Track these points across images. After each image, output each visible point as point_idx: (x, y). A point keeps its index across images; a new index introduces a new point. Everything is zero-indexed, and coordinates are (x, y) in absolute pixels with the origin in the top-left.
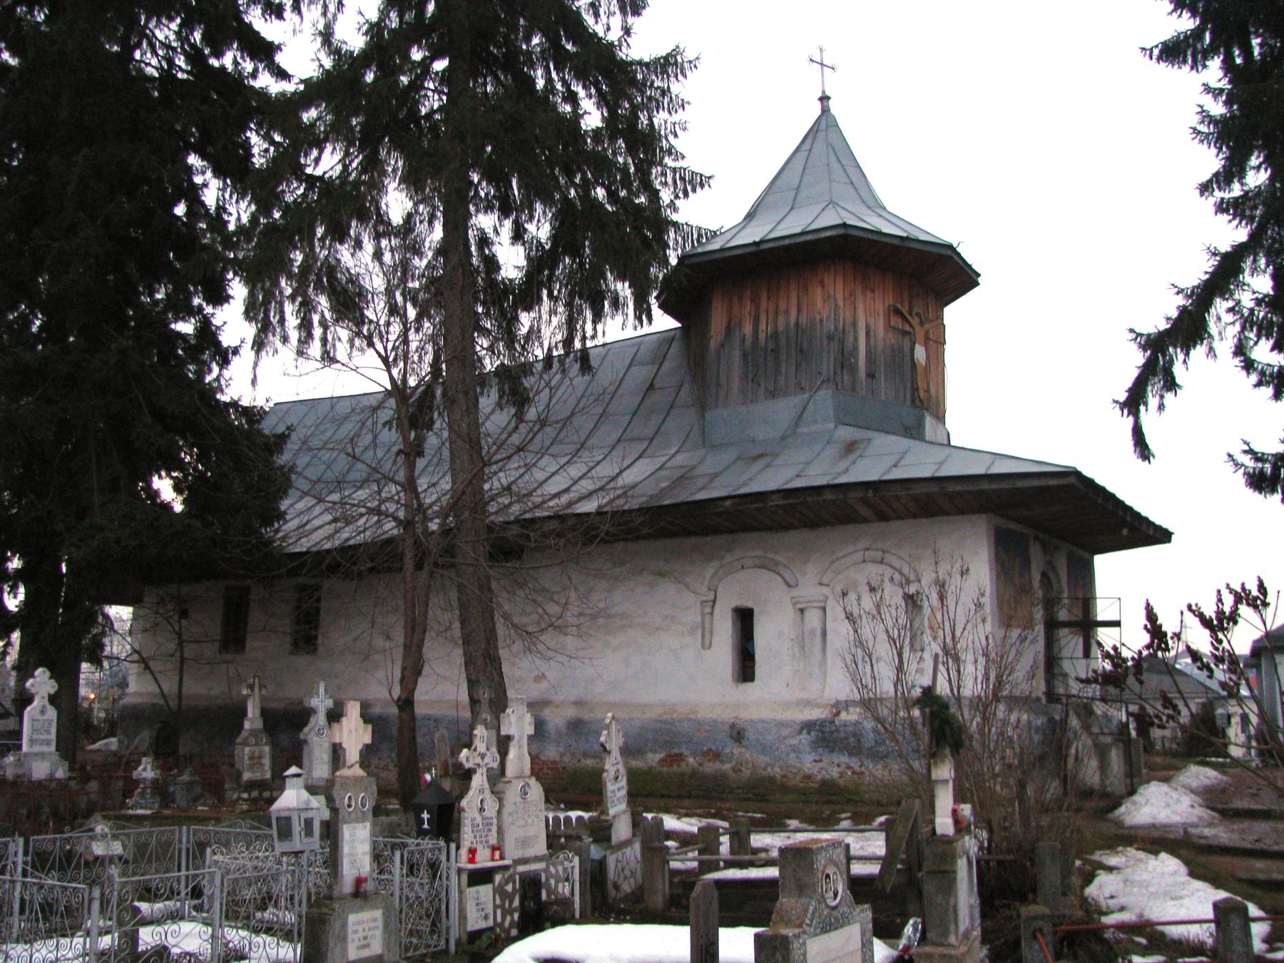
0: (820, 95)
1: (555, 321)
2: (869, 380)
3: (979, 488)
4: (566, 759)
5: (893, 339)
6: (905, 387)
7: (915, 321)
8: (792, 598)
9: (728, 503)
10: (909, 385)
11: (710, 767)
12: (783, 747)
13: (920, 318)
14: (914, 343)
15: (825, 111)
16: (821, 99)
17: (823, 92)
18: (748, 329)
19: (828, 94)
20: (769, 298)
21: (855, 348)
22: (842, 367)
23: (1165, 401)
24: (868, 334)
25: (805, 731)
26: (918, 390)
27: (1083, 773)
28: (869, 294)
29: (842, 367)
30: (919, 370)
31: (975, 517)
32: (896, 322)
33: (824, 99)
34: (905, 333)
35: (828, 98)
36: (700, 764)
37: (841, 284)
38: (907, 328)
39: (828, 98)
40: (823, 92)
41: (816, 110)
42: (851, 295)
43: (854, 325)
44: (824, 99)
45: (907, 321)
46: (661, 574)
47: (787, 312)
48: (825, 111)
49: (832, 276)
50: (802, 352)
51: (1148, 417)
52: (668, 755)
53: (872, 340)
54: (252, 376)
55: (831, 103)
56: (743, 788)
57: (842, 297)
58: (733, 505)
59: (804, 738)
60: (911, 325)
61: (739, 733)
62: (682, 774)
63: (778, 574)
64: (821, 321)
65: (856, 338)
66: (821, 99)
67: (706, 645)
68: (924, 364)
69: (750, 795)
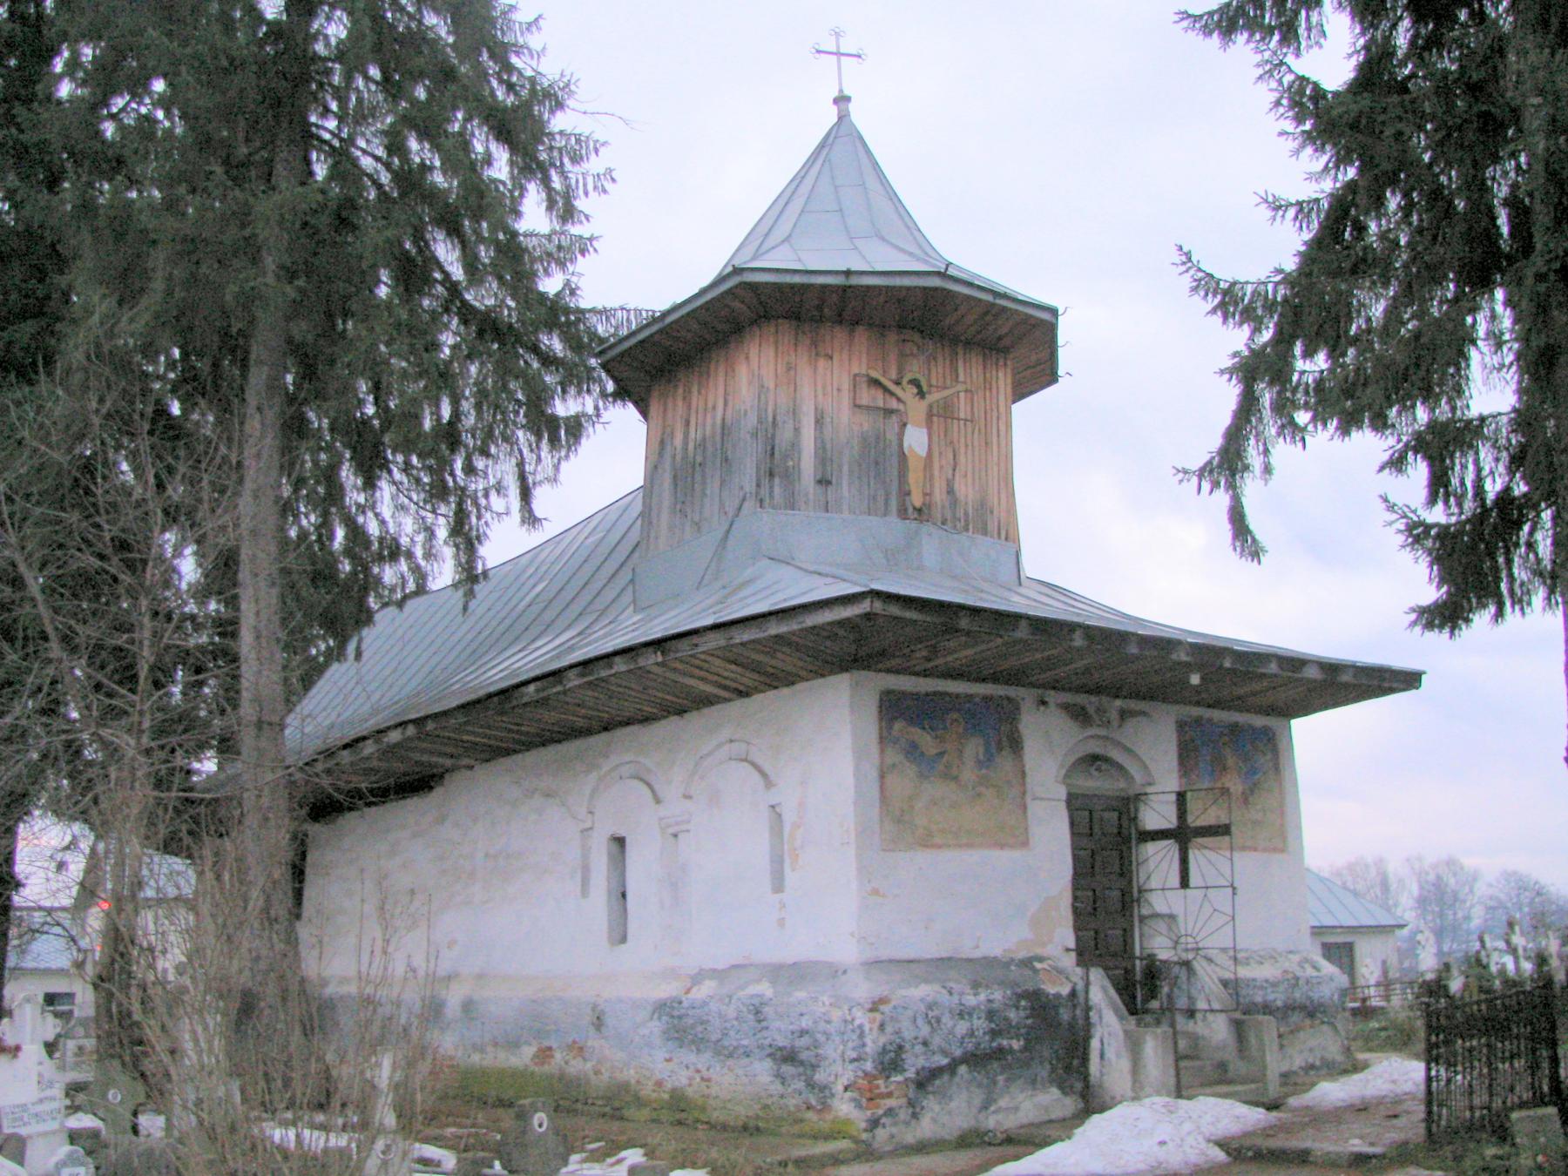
0: (835, 94)
2: (820, 490)
4: (460, 1054)
5: (866, 423)
8: (661, 819)
9: (532, 688)
10: (895, 484)
11: (576, 1067)
12: (637, 1038)
13: (919, 386)
14: (905, 425)
15: (843, 117)
17: (841, 91)
19: (847, 93)
21: (795, 446)
22: (771, 475)
23: (1273, 460)
25: (656, 1016)
26: (909, 493)
28: (822, 363)
29: (771, 475)
30: (912, 463)
31: (833, 679)
32: (867, 396)
33: (842, 100)
34: (889, 412)
35: (848, 99)
37: (772, 358)
38: (894, 404)
40: (841, 91)
43: (795, 412)
44: (842, 100)
45: (892, 394)
47: (714, 408)
48: (843, 117)
49: (757, 341)
50: (727, 460)
51: (1252, 489)
53: (828, 430)
54: (816, 576)
55: (852, 107)
57: (772, 374)
58: (537, 691)
60: (899, 399)
61: (405, 1030)
62: (552, 1076)
63: (648, 785)
64: (746, 411)
65: (797, 430)
66: (836, 101)
67: (585, 891)
68: (923, 452)
69: (607, 1109)
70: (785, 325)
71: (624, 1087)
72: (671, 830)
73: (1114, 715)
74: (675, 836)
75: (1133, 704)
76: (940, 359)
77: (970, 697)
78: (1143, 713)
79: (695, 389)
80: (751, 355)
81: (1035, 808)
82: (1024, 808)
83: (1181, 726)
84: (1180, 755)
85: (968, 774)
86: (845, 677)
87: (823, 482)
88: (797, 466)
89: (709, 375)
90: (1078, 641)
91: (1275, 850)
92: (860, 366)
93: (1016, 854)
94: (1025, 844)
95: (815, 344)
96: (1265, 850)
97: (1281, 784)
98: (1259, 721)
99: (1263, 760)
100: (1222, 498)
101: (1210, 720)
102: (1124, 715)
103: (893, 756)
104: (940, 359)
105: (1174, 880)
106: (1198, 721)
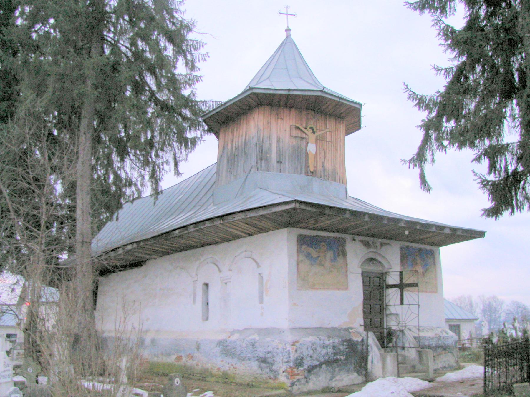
0: (286, 28)
1: (5, 150)
3: (259, 214)
5: (294, 142)
6: (301, 167)
7: (309, 132)
8: (221, 277)
10: (304, 165)
11: (190, 363)
13: (313, 130)
14: (308, 143)
15: (288, 36)
16: (286, 31)
17: (288, 27)
18: (229, 147)
19: (290, 28)
20: (237, 130)
21: (270, 149)
22: (261, 159)
23: (435, 157)
24: (278, 141)
26: (309, 167)
27: (121, 379)
29: (261, 159)
30: (310, 156)
32: (295, 133)
33: (288, 30)
34: (302, 138)
35: (290, 30)
36: (187, 361)
38: (304, 136)
39: (290, 30)
40: (288, 27)
41: (284, 35)
42: (268, 123)
43: (270, 138)
44: (288, 30)
45: (303, 132)
46: (182, 268)
47: (242, 136)
48: (288, 36)
50: (246, 154)
51: (427, 167)
52: (177, 357)
53: (281, 144)
55: (292, 33)
56: (199, 374)
58: (179, 232)
59: (218, 349)
64: (253, 137)
65: (270, 144)
66: (286, 31)
69: (201, 378)
70: (267, 108)
71: (206, 370)
72: (225, 282)
73: (378, 245)
74: (226, 283)
75: (385, 241)
76: (320, 120)
77: (329, 237)
78: (389, 244)
79: (235, 129)
80: (255, 118)
81: (350, 276)
82: (347, 276)
83: (402, 249)
84: (401, 259)
85: (328, 264)
86: (286, 229)
87: (279, 162)
88: (270, 157)
89: (240, 125)
90: (367, 219)
91: (433, 292)
92: (293, 122)
93: (343, 292)
94: (347, 289)
95: (277, 114)
96: (430, 292)
97: (436, 270)
98: (428, 247)
99: (430, 261)
100: (417, 170)
101: (412, 247)
102: (382, 244)
103: (302, 257)
104: (320, 120)
105: (398, 301)
106: (408, 247)
